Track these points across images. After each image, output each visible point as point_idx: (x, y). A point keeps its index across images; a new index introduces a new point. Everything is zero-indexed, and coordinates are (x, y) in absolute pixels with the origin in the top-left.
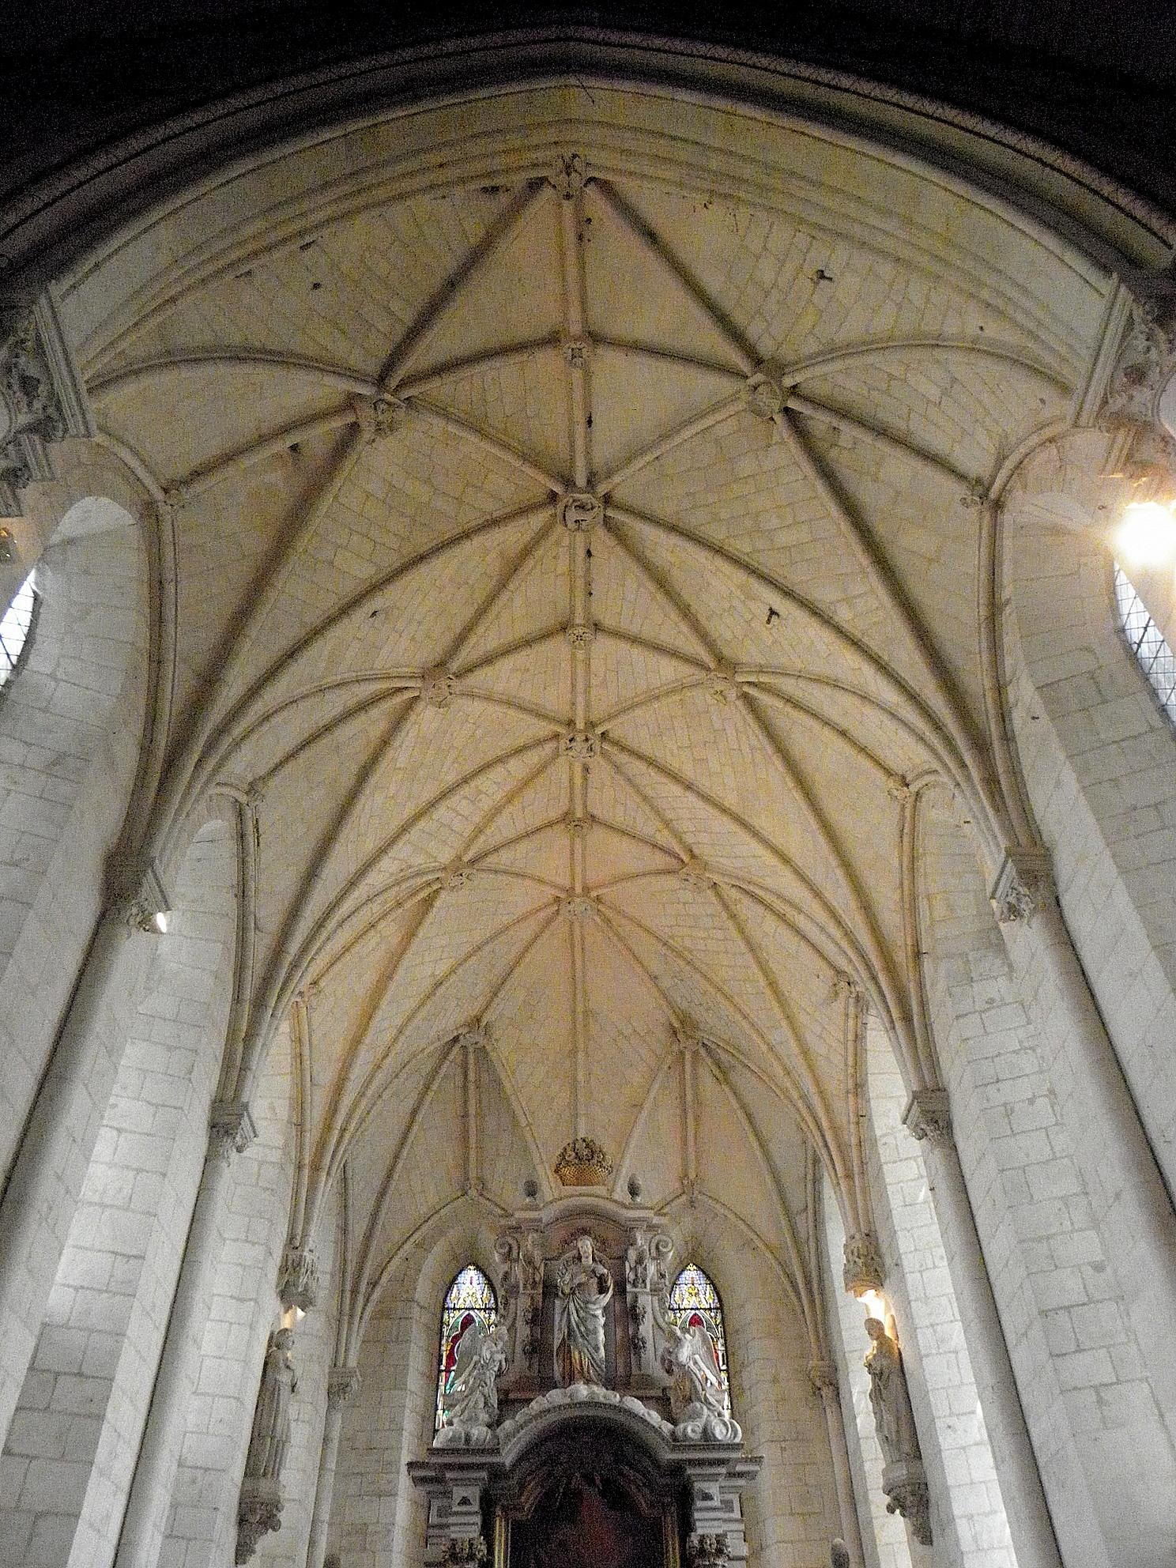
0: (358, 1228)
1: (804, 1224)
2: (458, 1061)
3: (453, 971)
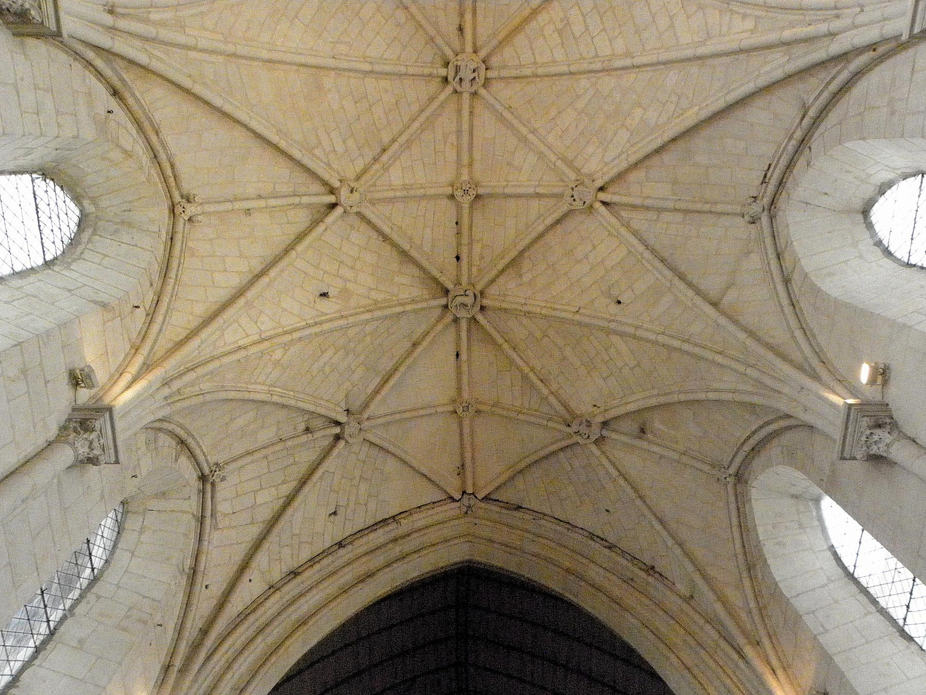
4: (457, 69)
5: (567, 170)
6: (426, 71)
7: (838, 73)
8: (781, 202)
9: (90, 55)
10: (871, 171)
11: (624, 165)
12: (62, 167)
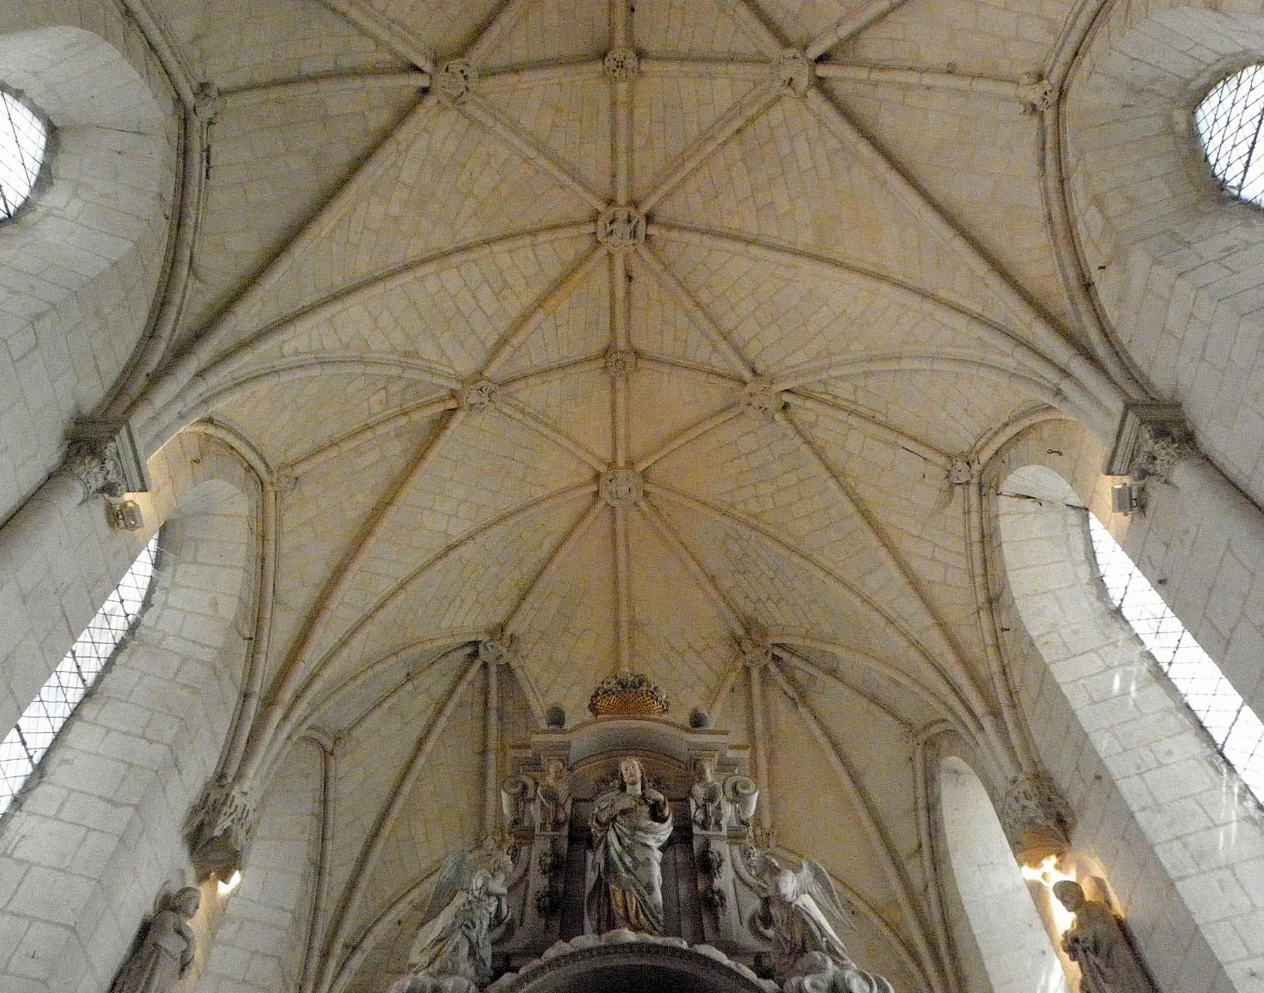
0: (338, 875)
1: (917, 871)
2: (478, 684)
3: (471, 537)
4: (634, 234)
5: (479, 115)
6: (674, 235)
7: (174, 330)
8: (174, 126)
9: (1101, 352)
10: (75, 205)
11: (402, 135)
12: (1194, 197)
